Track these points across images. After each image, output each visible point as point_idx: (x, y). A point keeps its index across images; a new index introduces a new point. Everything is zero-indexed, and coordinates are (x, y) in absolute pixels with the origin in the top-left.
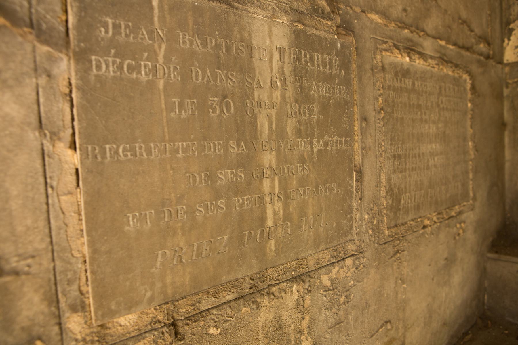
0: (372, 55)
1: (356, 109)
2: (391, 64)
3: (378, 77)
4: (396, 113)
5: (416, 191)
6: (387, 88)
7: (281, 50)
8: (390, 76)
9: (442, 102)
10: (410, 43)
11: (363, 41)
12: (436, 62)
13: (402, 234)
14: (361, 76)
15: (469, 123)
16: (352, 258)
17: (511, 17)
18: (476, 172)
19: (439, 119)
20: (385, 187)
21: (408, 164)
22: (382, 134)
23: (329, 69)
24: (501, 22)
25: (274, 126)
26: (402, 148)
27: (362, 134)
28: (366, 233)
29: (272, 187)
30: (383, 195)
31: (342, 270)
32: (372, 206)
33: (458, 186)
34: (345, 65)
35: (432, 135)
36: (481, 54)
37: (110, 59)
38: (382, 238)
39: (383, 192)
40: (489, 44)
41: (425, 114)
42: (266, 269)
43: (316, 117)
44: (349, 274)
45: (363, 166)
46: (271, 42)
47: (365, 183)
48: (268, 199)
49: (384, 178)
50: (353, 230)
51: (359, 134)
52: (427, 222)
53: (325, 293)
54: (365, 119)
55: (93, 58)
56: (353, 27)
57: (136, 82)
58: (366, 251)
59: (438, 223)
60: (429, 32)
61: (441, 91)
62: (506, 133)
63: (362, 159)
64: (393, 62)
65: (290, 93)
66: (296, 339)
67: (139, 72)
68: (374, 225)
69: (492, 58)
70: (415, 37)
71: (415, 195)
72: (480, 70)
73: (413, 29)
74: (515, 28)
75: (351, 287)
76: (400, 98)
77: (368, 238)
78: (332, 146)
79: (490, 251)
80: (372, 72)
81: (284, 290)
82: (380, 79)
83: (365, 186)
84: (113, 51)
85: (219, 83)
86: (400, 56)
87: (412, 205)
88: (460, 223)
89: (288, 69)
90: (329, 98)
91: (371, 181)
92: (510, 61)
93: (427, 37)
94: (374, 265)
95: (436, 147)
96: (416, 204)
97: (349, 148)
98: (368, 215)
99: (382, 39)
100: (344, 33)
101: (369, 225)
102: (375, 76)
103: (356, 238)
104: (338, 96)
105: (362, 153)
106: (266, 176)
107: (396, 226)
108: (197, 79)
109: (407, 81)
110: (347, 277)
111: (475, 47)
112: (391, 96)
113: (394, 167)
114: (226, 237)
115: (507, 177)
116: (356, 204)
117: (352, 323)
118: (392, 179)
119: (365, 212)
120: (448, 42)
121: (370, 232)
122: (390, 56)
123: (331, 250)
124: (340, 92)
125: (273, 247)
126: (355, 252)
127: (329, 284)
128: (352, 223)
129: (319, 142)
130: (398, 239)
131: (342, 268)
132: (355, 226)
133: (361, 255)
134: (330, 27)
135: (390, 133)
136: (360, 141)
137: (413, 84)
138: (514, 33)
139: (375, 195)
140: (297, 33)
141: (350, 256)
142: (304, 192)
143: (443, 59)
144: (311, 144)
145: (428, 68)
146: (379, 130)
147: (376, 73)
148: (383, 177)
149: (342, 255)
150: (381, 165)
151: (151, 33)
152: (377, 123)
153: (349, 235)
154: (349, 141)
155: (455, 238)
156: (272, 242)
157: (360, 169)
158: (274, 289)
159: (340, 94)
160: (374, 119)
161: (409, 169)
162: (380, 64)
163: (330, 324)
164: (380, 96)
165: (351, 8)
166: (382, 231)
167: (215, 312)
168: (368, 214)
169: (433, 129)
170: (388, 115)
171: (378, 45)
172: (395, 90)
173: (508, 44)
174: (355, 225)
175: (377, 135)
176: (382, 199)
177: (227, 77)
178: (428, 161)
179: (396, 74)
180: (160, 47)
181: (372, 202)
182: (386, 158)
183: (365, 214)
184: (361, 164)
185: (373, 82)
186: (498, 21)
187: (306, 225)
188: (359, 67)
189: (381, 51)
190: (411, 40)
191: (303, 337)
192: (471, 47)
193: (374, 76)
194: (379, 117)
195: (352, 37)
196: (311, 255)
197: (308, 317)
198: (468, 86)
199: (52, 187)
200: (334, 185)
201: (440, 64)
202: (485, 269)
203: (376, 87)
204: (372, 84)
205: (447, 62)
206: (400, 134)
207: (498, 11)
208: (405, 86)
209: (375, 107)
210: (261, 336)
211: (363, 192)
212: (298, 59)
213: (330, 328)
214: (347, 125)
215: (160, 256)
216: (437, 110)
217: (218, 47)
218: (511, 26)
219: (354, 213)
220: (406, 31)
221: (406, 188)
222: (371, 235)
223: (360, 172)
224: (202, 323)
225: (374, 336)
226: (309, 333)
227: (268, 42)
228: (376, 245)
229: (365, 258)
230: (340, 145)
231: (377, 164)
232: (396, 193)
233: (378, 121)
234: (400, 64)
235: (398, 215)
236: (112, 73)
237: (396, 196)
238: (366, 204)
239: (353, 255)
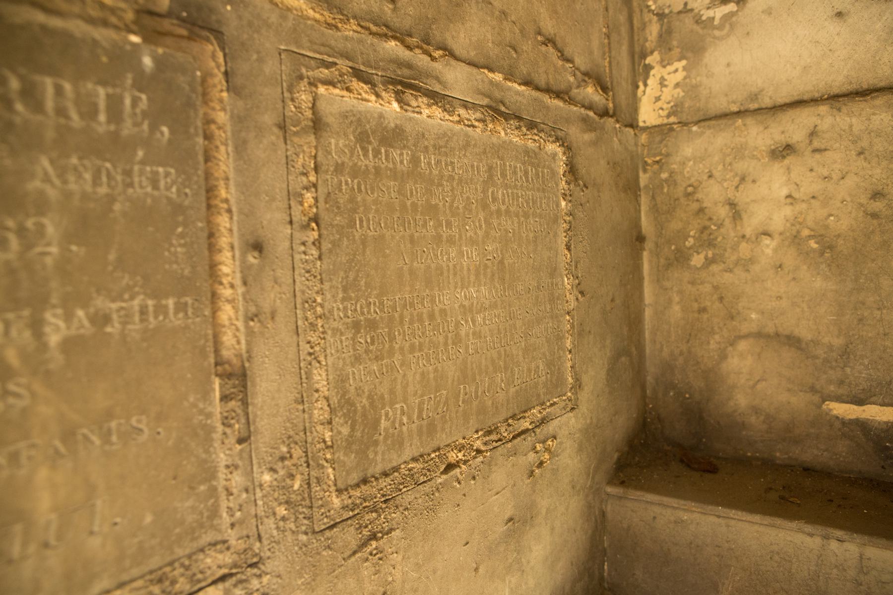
0: (283, 93)
2: (344, 115)
3: (302, 143)
4: (361, 226)
5: (422, 396)
6: (332, 169)
8: (341, 142)
9: (495, 199)
10: (406, 72)
11: (255, 57)
12: (478, 115)
13: (383, 496)
14: (245, 142)
15: (562, 240)
16: (220, 586)
17: (647, 44)
18: (580, 333)
19: (487, 235)
20: (327, 399)
21: (399, 339)
22: (315, 277)
23: (109, 121)
24: (632, 54)
26: (382, 303)
27: (245, 283)
28: (267, 517)
30: (321, 417)
32: (284, 449)
33: (538, 367)
35: (469, 269)
36: (590, 107)
38: (322, 517)
39: (321, 412)
40: (605, 89)
41: (449, 224)
43: (54, 250)
45: (250, 358)
47: (259, 400)
49: (323, 380)
50: (221, 517)
51: (238, 282)
52: (453, 456)
56: (219, 22)
58: (269, 558)
59: (487, 451)
60: (458, 51)
61: (491, 177)
62: (645, 254)
63: (248, 343)
64: (352, 111)
68: (295, 491)
69: (612, 117)
70: (420, 59)
71: (421, 403)
72: (588, 137)
73: (414, 41)
74: (654, 64)
75: (577, 72)
76: (372, 193)
77: (273, 526)
79: (610, 482)
80: (281, 134)
82: (305, 148)
83: (260, 405)
86: (373, 98)
87: (414, 426)
88: (544, 442)
90: (111, 199)
91: (279, 391)
92: (648, 124)
93: (453, 62)
94: (300, 582)
95: (481, 293)
96: (425, 423)
97: (193, 323)
98: (271, 473)
99: (318, 56)
100: (184, 32)
101: (276, 495)
102: (292, 141)
103: (232, 536)
104: (146, 194)
105: (247, 327)
107: (365, 481)
109: (395, 154)
111: (575, 91)
112: (344, 187)
113: (355, 350)
115: (647, 335)
116: (226, 455)
118: (351, 377)
119: (260, 467)
120: (510, 76)
122: (343, 97)
126: (231, 569)
128: (216, 502)
130: (374, 510)
132: (228, 508)
135: (342, 274)
136: (240, 298)
137: (415, 161)
138: (652, 72)
139: (295, 421)
141: (214, 582)
143: (496, 111)
145: (458, 127)
146: (304, 269)
147: (296, 134)
148: (320, 378)
150: (311, 351)
152: (299, 253)
153: (206, 533)
154: (193, 304)
155: (531, 474)
157: (243, 366)
159: (156, 187)
160: (287, 244)
161: (401, 349)
162: (309, 114)
164: (307, 188)
166: (320, 502)
168: (273, 470)
169: (471, 256)
170: (335, 232)
171: (304, 70)
172: (355, 172)
173: (644, 92)
175: (297, 281)
176: (320, 428)
178: (458, 324)
179: (363, 138)
181: (285, 439)
182: (329, 332)
183: (262, 472)
184: (245, 355)
185: (287, 157)
186: (625, 48)
187: (25, 544)
188: (239, 120)
189: (312, 84)
190: (409, 66)
192: (567, 92)
193: (288, 142)
194: (305, 239)
195: (212, 44)
198: (561, 168)
201: (488, 119)
202: (603, 514)
203: (293, 167)
204: (284, 161)
205: (507, 117)
206: (373, 272)
207: (624, 30)
208: (391, 165)
209: (290, 215)
211: (254, 422)
214: (183, 266)
216: (481, 216)
218: (648, 60)
219: (222, 474)
220: (393, 43)
221: (392, 392)
229: (267, 574)
230: (156, 317)
231: (301, 348)
232: (364, 407)
233: (303, 248)
234: (376, 115)
235: (371, 456)
237: (364, 415)
238: (264, 449)
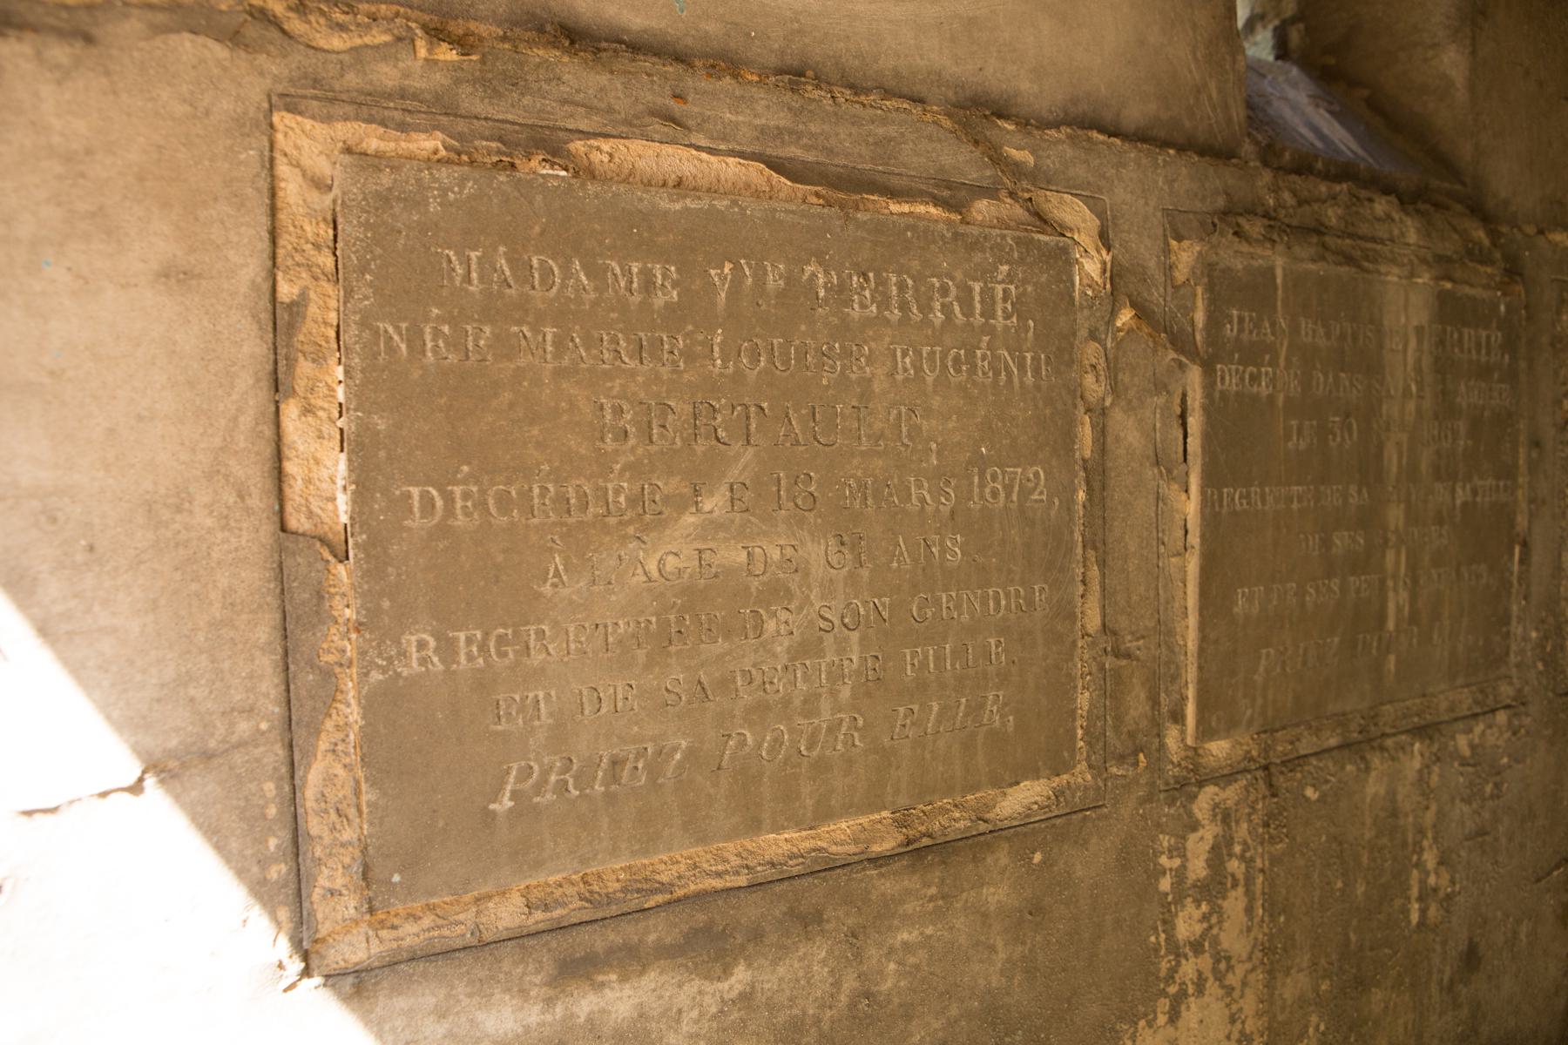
1: (1522, 426)
7: (1419, 330)
16: (1508, 711)
25: (1404, 461)
29: (1397, 563)
31: (1489, 731)
34: (1509, 346)
37: (1234, 367)
42: (1382, 704)
44: (1500, 742)
46: (1407, 318)
48: (1390, 583)
53: (1461, 769)
54: (1537, 444)
55: (1219, 366)
57: (1255, 398)
65: (1427, 404)
66: (1415, 844)
67: (1260, 385)
78: (1484, 496)
81: (1403, 748)
84: (1237, 356)
85: (1342, 394)
89: (1427, 362)
106: (1390, 544)
108: (1318, 389)
110: (1498, 747)
114: (1336, 640)
117: (1504, 840)
121: (1540, 666)
123: (1474, 688)
124: (1500, 394)
125: (1392, 667)
127: (1466, 752)
129: (1464, 488)
131: (1490, 727)
133: (1522, 709)
134: (1491, 276)
140: (1443, 298)
142: (1439, 575)
144: (1453, 492)
149: (1490, 701)
151: (1273, 324)
156: (1392, 658)
158: (1389, 742)
163: (1467, 831)
165: (1520, 229)
167: (1314, 761)
174: (1514, 647)
177: (1352, 384)
180: (1282, 344)
191: (1425, 843)
196: (1442, 692)
197: (1434, 808)
199: (1163, 543)
200: (1483, 568)
210: (1369, 821)
212: (1441, 343)
213: (1467, 839)
215: (1264, 657)
217: (1342, 337)
222: (1541, 673)
223: (1525, 545)
224: (1299, 775)
225: (1544, 882)
226: (1435, 839)
227: (1403, 320)
228: (1550, 694)
236: (1235, 388)
239: (1508, 707)
